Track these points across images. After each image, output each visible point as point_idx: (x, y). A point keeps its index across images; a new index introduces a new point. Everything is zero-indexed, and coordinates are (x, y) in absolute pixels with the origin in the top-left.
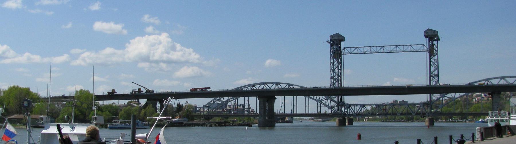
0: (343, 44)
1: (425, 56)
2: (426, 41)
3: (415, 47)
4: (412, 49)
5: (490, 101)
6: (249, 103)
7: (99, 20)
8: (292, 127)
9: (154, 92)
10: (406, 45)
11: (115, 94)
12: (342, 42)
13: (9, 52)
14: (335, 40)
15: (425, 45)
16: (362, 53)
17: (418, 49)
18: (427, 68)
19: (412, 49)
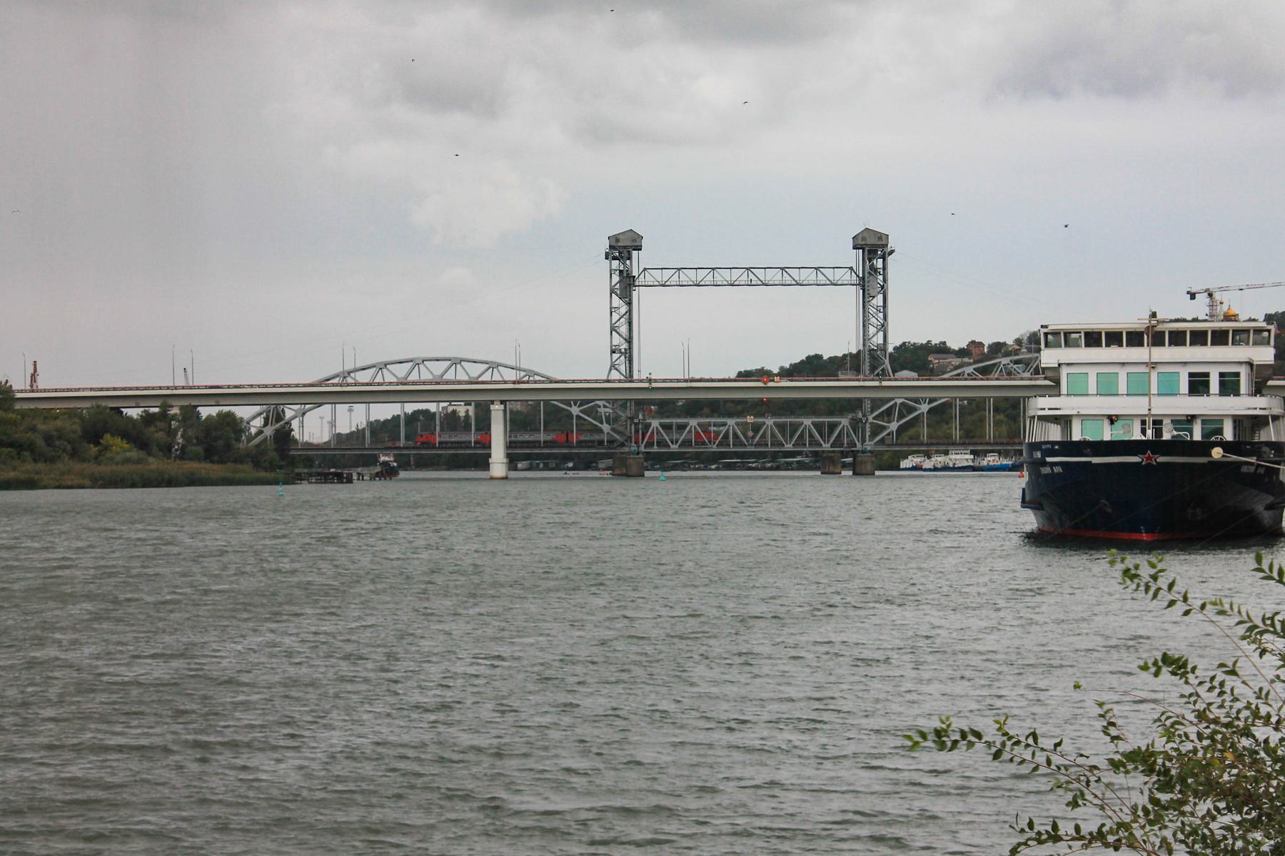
0: (639, 261)
1: (851, 295)
2: (853, 258)
3: (828, 272)
4: (822, 277)
5: (850, 417)
6: (593, 820)
7: (157, 413)
8: (319, 587)
9: (825, 358)
10: (752, 277)
11: (986, 351)
12: (635, 253)
13: (1120, 584)
14: (625, 247)
15: (855, 269)
16: (657, 284)
17: (837, 278)
18: (56, 390)
19: (821, 277)
